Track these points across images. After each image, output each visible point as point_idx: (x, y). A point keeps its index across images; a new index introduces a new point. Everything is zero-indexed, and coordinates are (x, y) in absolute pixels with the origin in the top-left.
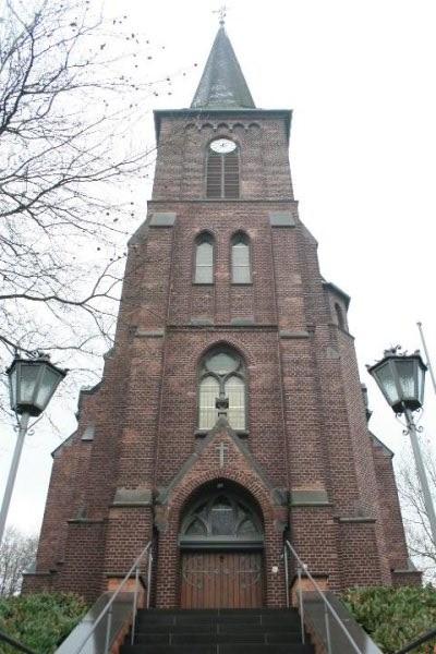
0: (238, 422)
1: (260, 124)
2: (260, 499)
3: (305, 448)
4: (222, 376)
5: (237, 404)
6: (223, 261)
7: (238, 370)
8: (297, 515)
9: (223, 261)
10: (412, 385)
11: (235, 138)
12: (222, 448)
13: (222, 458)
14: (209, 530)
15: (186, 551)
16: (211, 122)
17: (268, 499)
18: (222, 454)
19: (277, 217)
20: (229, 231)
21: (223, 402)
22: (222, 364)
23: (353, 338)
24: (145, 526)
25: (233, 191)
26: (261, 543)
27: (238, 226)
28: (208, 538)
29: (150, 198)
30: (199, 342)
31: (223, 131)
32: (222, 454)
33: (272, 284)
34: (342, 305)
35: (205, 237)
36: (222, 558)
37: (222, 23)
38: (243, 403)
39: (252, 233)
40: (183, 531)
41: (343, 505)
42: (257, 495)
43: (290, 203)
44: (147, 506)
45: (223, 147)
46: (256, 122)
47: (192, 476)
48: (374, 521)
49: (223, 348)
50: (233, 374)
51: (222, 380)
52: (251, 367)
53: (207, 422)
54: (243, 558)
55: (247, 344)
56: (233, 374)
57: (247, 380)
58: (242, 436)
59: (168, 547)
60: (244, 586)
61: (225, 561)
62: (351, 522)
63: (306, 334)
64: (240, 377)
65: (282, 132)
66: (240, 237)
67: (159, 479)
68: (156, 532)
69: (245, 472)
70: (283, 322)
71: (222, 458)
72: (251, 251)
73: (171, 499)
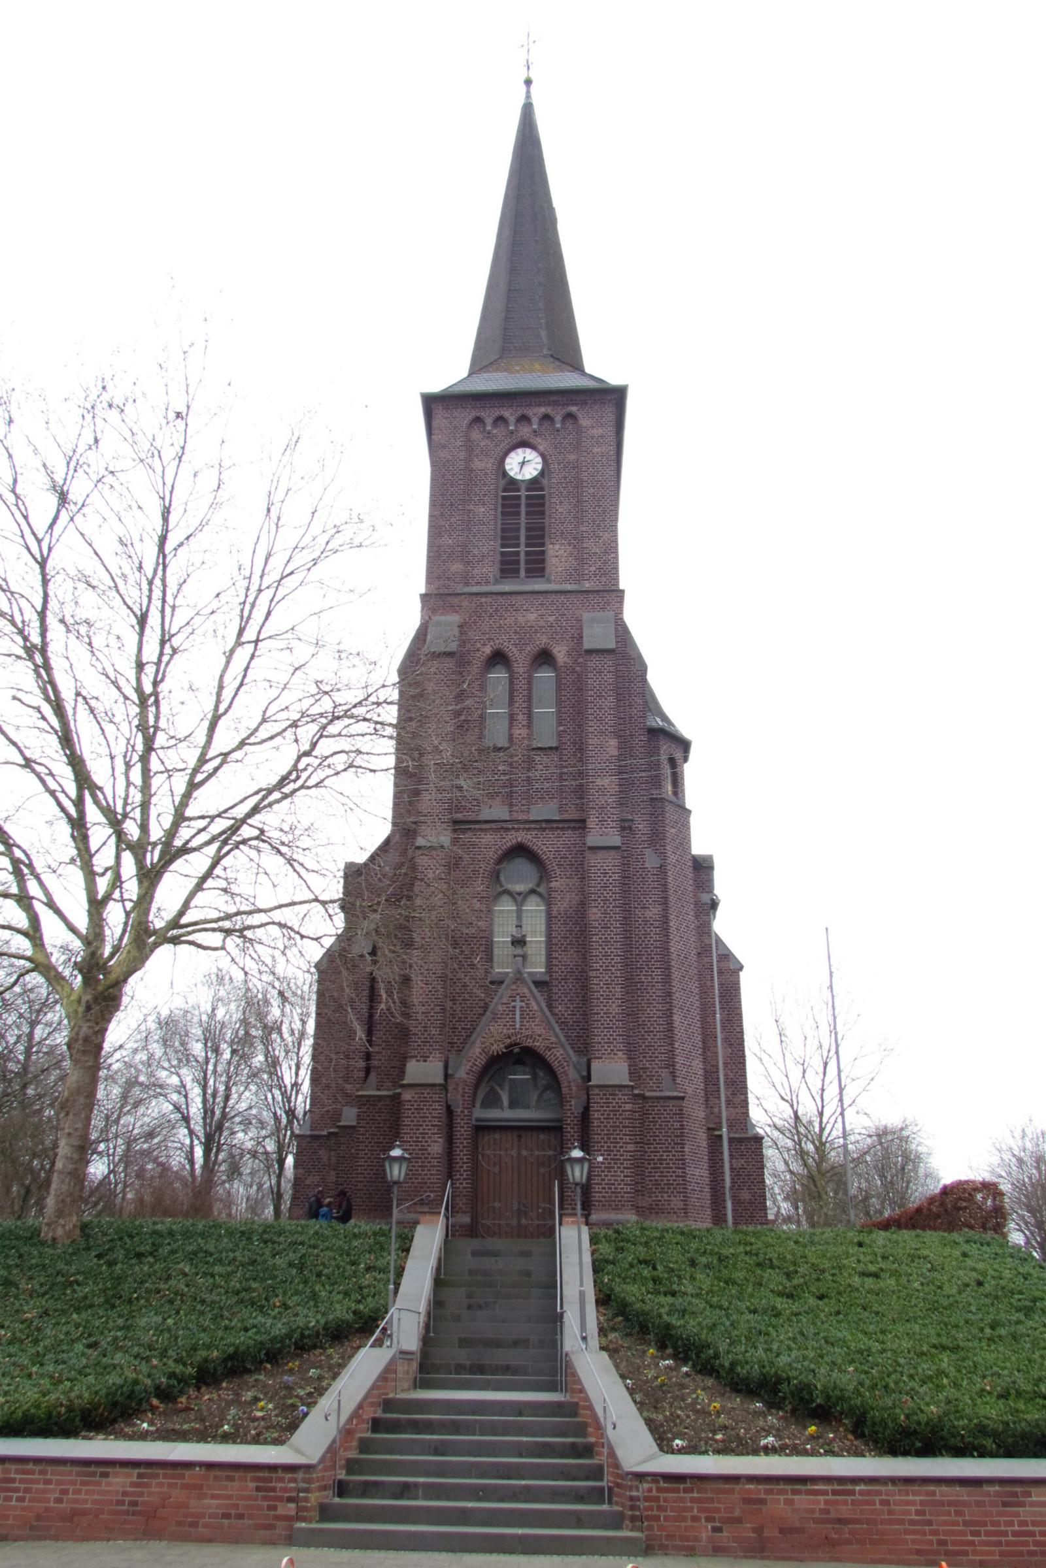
0: (537, 967)
1: (579, 415)
2: (559, 1071)
3: (608, 1004)
4: (519, 894)
5: (536, 938)
6: (520, 699)
7: (538, 885)
8: (597, 1097)
9: (520, 699)
10: (638, 1400)
11: (541, 448)
12: (518, 1004)
13: (518, 1016)
14: (506, 1102)
15: (481, 1129)
16: (506, 414)
17: (570, 1076)
18: (518, 1013)
19: (597, 636)
20: (531, 649)
21: (521, 927)
22: (520, 877)
23: (689, 812)
24: (438, 1109)
25: (537, 567)
26: (560, 1120)
27: (542, 640)
28: (504, 1113)
29: (423, 591)
30: (491, 843)
31: (525, 431)
32: (518, 1013)
33: (580, 748)
34: (678, 755)
35: (499, 658)
36: (519, 1137)
37: (528, 82)
38: (544, 964)
39: (561, 653)
40: (478, 1105)
41: (651, 1077)
42: (555, 1065)
43: (611, 596)
44: (440, 1085)
45: (524, 465)
46: (574, 409)
47: (491, 1037)
48: (683, 1098)
49: (521, 851)
50: (533, 891)
51: (519, 899)
52: (553, 885)
53: (503, 966)
54: (542, 1137)
55: (546, 845)
56: (533, 891)
57: (548, 901)
58: (538, 984)
59: (463, 1131)
60: (542, 1170)
61: (523, 1140)
62: (658, 1098)
63: (616, 840)
64: (540, 895)
65: (610, 431)
66: (544, 657)
67: (455, 1045)
68: (449, 1110)
69: (543, 1033)
70: (592, 822)
71: (518, 1016)
72: (558, 679)
73: (463, 1072)
